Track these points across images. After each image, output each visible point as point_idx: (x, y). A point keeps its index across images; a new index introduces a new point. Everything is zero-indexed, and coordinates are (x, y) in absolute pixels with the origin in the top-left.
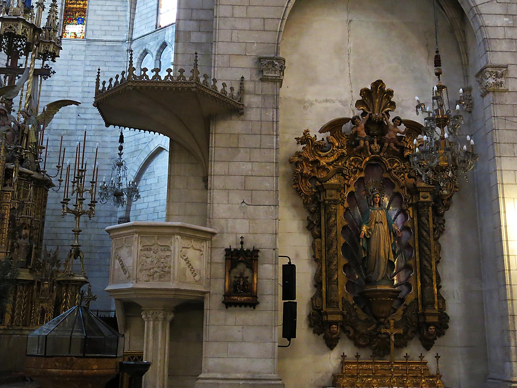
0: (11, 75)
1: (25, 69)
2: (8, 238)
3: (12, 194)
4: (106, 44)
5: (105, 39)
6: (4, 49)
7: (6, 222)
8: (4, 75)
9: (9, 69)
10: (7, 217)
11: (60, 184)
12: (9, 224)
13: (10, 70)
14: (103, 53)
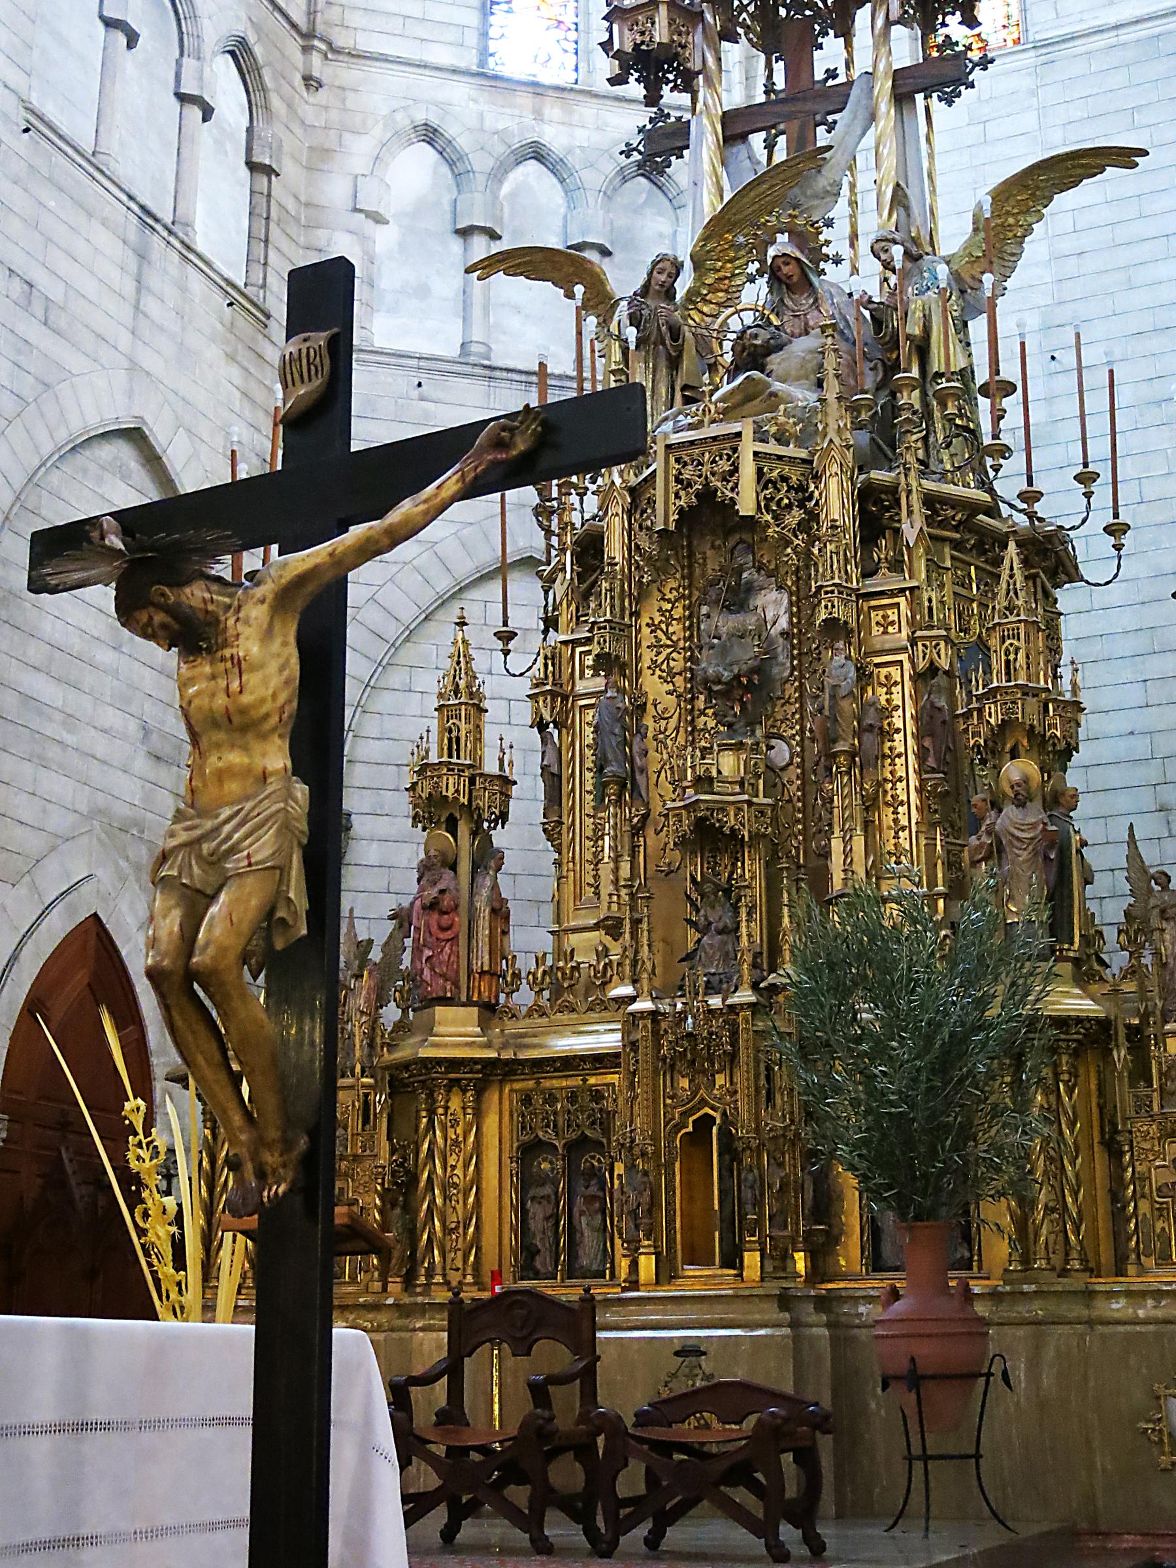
0: (796, 124)
1: (850, 84)
2: (928, 825)
3: (911, 603)
4: (1123, 39)
5: (1112, 20)
6: (748, 29)
7: (904, 743)
8: (762, 135)
9: (783, 101)
10: (904, 719)
11: (1118, 547)
12: (921, 756)
13: (786, 108)
14: (1118, 79)
